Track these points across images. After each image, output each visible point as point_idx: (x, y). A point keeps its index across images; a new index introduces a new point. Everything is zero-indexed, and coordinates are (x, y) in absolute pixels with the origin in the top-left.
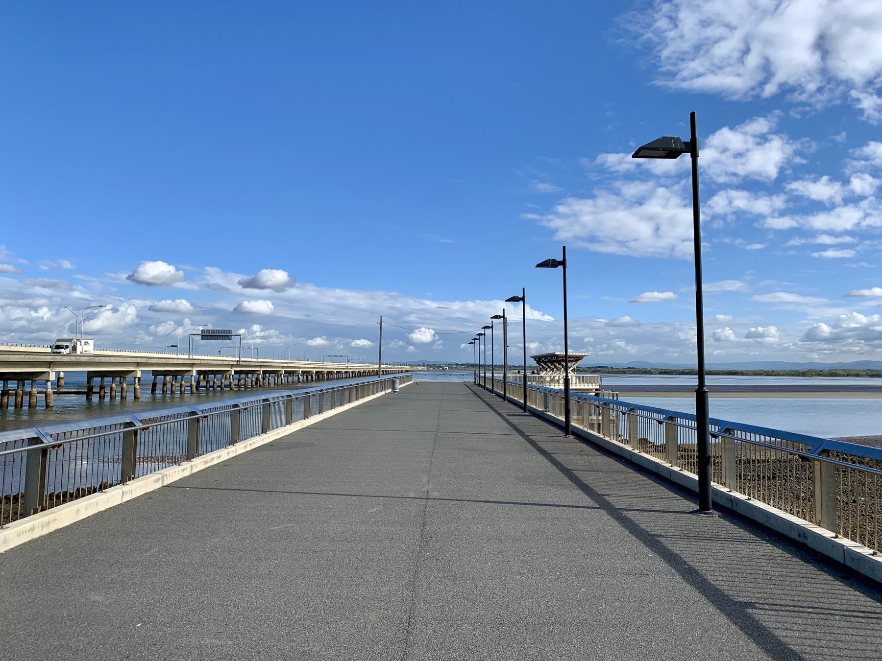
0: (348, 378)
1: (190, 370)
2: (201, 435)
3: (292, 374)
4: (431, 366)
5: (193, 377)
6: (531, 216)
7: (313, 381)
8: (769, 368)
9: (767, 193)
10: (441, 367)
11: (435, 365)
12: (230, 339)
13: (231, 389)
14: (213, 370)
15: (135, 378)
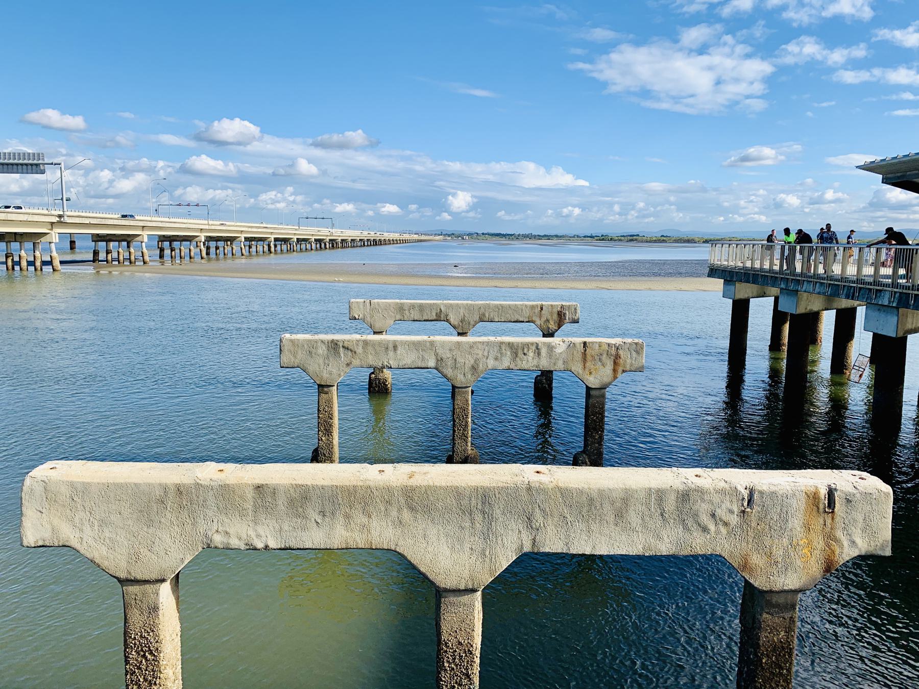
0: (309, 251)
3: (229, 243)
4: (449, 235)
6: (580, 65)
7: (271, 253)
8: (504, 241)
10: (460, 237)
11: (453, 234)
12: (43, 172)
14: (15, 234)
15: (50, 243)
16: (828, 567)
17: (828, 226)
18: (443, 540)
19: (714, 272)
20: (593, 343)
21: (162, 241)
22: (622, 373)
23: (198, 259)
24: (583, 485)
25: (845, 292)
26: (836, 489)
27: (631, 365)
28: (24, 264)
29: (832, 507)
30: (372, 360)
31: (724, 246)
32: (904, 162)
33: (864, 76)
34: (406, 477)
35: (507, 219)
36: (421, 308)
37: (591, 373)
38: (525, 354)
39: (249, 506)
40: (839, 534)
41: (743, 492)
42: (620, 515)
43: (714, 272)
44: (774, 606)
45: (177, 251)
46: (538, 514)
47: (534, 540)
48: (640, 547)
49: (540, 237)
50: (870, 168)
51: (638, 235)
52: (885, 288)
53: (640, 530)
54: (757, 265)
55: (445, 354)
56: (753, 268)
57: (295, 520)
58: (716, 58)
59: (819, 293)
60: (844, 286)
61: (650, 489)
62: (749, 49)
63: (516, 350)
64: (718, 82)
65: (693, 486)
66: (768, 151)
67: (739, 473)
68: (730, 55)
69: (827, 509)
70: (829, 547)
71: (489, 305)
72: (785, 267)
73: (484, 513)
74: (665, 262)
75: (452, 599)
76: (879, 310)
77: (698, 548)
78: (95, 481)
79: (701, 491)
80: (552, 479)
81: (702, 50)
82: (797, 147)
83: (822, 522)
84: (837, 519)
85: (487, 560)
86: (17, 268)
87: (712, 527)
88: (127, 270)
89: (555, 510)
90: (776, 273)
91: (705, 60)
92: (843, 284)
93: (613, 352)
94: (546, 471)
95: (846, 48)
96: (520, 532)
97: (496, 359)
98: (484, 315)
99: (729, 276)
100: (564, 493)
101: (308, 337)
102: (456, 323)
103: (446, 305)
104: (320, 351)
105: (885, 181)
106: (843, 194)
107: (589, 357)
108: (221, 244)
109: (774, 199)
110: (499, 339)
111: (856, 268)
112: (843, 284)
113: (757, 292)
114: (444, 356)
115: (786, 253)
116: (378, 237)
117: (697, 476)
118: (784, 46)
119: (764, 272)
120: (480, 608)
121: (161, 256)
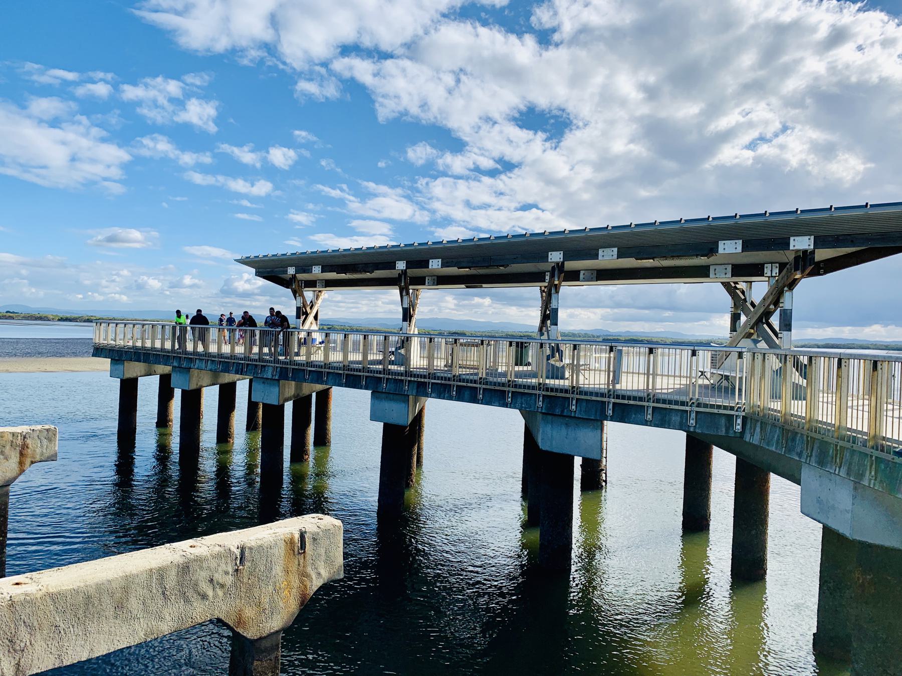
17: (199, 311)
19: (99, 351)
22: (30, 465)
24: (78, 585)
25: (234, 369)
26: (305, 532)
27: (42, 454)
29: (303, 548)
31: (111, 325)
32: (273, 260)
33: (209, 180)
35: (876, 327)
40: (309, 569)
41: (236, 552)
42: (120, 607)
43: (99, 351)
46: (23, 633)
47: (18, 664)
48: (142, 634)
50: (247, 262)
52: (268, 364)
53: (141, 616)
54: (148, 344)
56: (143, 348)
58: (70, 134)
60: (233, 363)
61: (151, 570)
62: (104, 133)
64: (73, 159)
65: (192, 557)
66: (136, 234)
67: (227, 536)
68: (86, 135)
69: (300, 552)
72: (177, 346)
74: (18, 341)
76: (263, 383)
77: (198, 617)
79: (199, 560)
80: (40, 586)
81: (55, 123)
82: (155, 234)
83: (297, 563)
84: (308, 557)
87: (210, 593)
89: (44, 622)
90: (168, 352)
91: (57, 133)
92: (233, 361)
93: (19, 441)
95: (194, 153)
100: (54, 598)
105: (259, 274)
106: (200, 280)
109: (136, 281)
111: (243, 348)
112: (233, 361)
113: (145, 370)
115: (178, 333)
117: (191, 547)
118: (138, 139)
119: (165, 352)
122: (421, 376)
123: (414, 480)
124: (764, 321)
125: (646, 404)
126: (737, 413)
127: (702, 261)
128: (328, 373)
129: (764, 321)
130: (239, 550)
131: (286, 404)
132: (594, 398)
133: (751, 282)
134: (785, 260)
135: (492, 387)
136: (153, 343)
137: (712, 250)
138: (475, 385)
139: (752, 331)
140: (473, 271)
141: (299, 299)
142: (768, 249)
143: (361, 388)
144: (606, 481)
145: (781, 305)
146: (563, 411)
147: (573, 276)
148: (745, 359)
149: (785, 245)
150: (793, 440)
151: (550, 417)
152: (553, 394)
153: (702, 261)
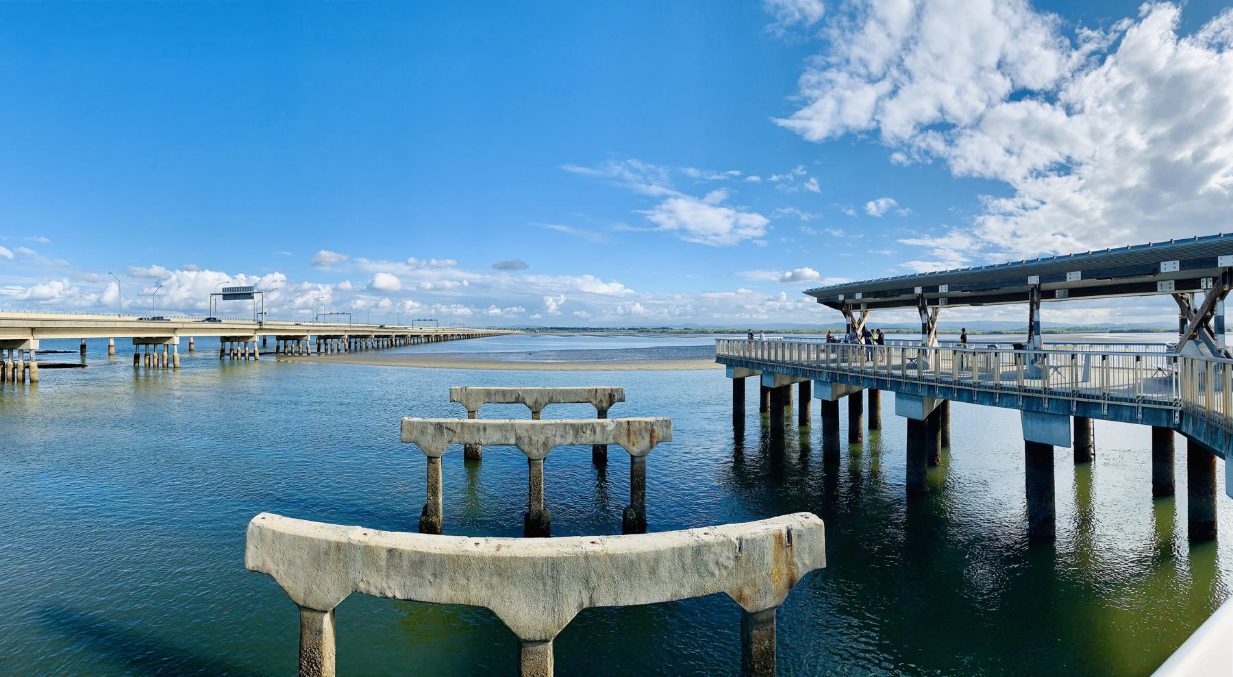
1: (171, 337)
2: (519, 368)
5: (176, 346)
9: (1118, 21)
12: (253, 298)
13: (256, 359)
16: (791, 584)
18: (523, 600)
20: (634, 422)
21: (319, 339)
23: (343, 351)
28: (239, 355)
30: (468, 439)
34: (494, 549)
36: (504, 393)
37: (634, 445)
38: (584, 432)
39: (383, 563)
40: (796, 560)
42: (653, 571)
43: (720, 359)
44: (759, 623)
45: (329, 346)
47: (591, 597)
48: (669, 595)
49: (595, 330)
50: (810, 293)
51: (668, 328)
53: (668, 581)
54: (747, 355)
55: (523, 434)
57: (414, 578)
59: (786, 374)
63: (577, 429)
70: (790, 570)
71: (555, 390)
73: (553, 578)
75: (531, 648)
78: (288, 533)
83: (785, 554)
84: (795, 550)
85: (557, 616)
86: (236, 358)
87: (717, 572)
88: (297, 359)
90: (766, 361)
94: (599, 541)
96: (580, 591)
97: (562, 436)
98: (552, 398)
99: (730, 362)
100: (612, 558)
101: (420, 420)
102: (531, 404)
103: (523, 391)
104: (429, 431)
105: (819, 301)
107: (631, 431)
108: (358, 339)
110: (564, 421)
114: (522, 436)
116: (471, 331)
120: (552, 654)
121: (319, 350)
122: (931, 381)
123: (940, 460)
124: (1204, 325)
125: (1102, 401)
126: (1175, 408)
127: (1150, 278)
128: (864, 377)
129: (1204, 325)
130: (738, 541)
131: (840, 400)
132: (1062, 398)
133: (1193, 293)
134: (1216, 274)
135: (984, 390)
136: (750, 354)
137: (1156, 270)
138: (970, 388)
139: (1195, 334)
140: (973, 294)
141: (849, 319)
142: (1201, 267)
143: (887, 390)
144: (1094, 455)
145: (1215, 313)
146: (1038, 409)
147: (1050, 294)
148: (1179, 363)
149: (1214, 262)
150: (1216, 434)
151: (1029, 413)
152: (1030, 394)
153: (1150, 278)
